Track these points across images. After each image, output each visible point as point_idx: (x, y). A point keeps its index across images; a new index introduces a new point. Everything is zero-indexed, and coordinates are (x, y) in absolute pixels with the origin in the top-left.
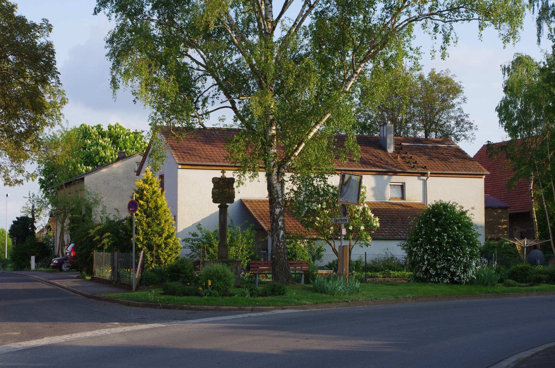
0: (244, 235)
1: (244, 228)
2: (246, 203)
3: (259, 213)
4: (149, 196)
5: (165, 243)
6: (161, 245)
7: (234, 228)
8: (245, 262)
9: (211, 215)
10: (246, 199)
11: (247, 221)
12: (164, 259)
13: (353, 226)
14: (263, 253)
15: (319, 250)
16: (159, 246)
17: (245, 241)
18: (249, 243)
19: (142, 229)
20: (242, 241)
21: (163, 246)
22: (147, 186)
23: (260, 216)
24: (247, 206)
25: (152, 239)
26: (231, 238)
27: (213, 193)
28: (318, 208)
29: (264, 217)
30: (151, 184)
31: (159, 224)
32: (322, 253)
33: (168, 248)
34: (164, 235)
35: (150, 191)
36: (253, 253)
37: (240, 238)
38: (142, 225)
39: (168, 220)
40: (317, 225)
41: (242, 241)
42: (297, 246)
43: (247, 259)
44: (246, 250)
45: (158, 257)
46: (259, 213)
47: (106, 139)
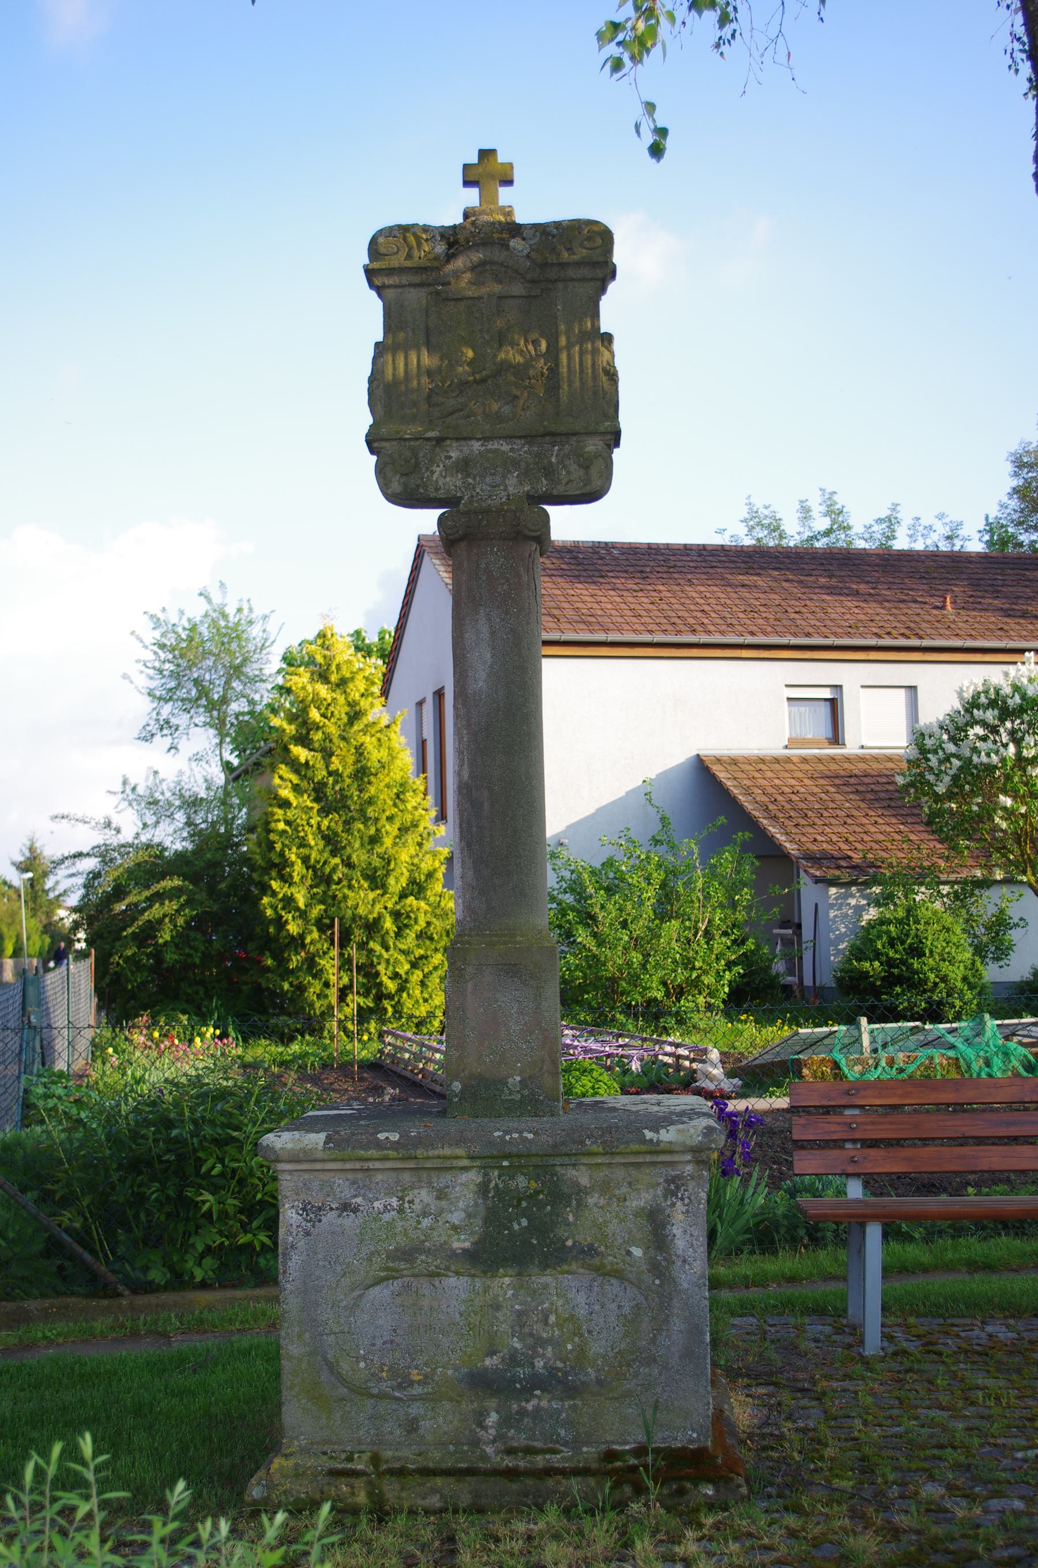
0: (712, 873)
1: (711, 846)
2: (716, 769)
3: (764, 799)
4: (333, 730)
5: (396, 915)
6: (378, 920)
7: (673, 848)
8: (719, 976)
9: (599, 810)
10: (717, 753)
11: (722, 820)
12: (396, 976)
13: (268, 969)
14: (783, 937)
15: (1000, 924)
16: (373, 927)
17: (719, 895)
18: (734, 905)
19: (305, 860)
20: (707, 897)
21: (388, 924)
22: (323, 690)
23: (767, 810)
24: (722, 775)
25: (345, 897)
26: (663, 885)
27: (383, 393)
28: (1003, 760)
29: (782, 810)
30: (343, 683)
31: (375, 840)
32: (1014, 935)
33: (411, 935)
34: (396, 883)
35: (341, 710)
36: (750, 945)
37: (699, 885)
38: (303, 844)
39: (415, 825)
40: (1004, 825)
41: (707, 897)
42: (923, 913)
43: (730, 965)
44: (725, 934)
45: (368, 971)
46: (764, 799)
47: (373, 660)
